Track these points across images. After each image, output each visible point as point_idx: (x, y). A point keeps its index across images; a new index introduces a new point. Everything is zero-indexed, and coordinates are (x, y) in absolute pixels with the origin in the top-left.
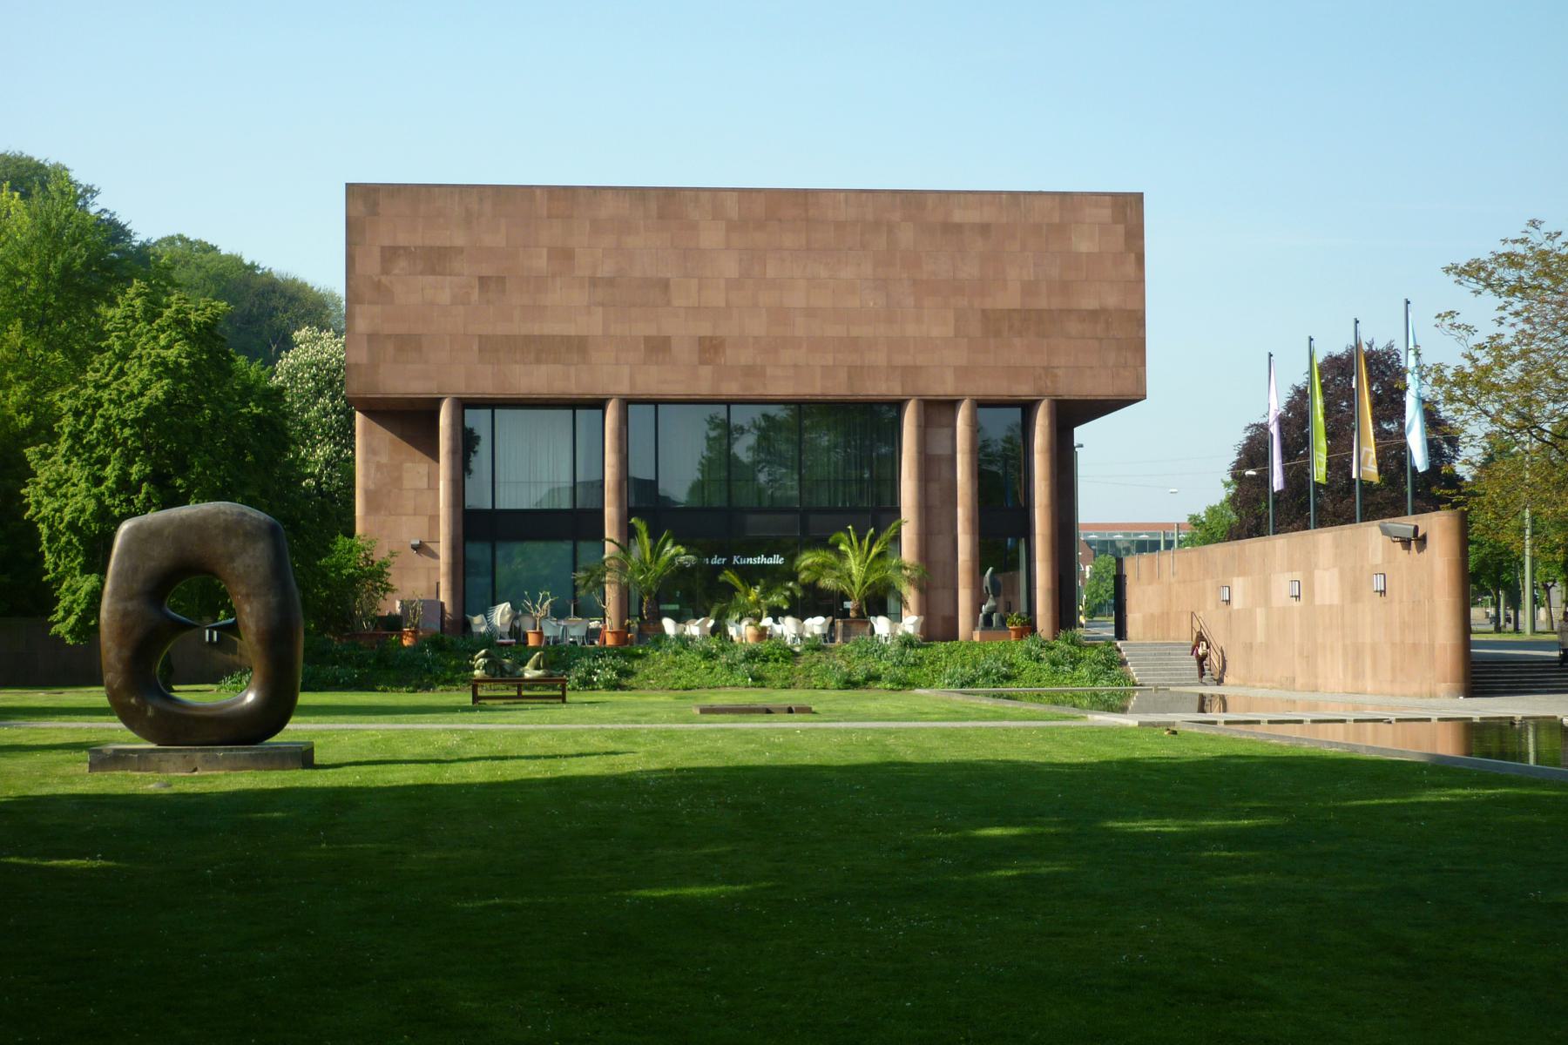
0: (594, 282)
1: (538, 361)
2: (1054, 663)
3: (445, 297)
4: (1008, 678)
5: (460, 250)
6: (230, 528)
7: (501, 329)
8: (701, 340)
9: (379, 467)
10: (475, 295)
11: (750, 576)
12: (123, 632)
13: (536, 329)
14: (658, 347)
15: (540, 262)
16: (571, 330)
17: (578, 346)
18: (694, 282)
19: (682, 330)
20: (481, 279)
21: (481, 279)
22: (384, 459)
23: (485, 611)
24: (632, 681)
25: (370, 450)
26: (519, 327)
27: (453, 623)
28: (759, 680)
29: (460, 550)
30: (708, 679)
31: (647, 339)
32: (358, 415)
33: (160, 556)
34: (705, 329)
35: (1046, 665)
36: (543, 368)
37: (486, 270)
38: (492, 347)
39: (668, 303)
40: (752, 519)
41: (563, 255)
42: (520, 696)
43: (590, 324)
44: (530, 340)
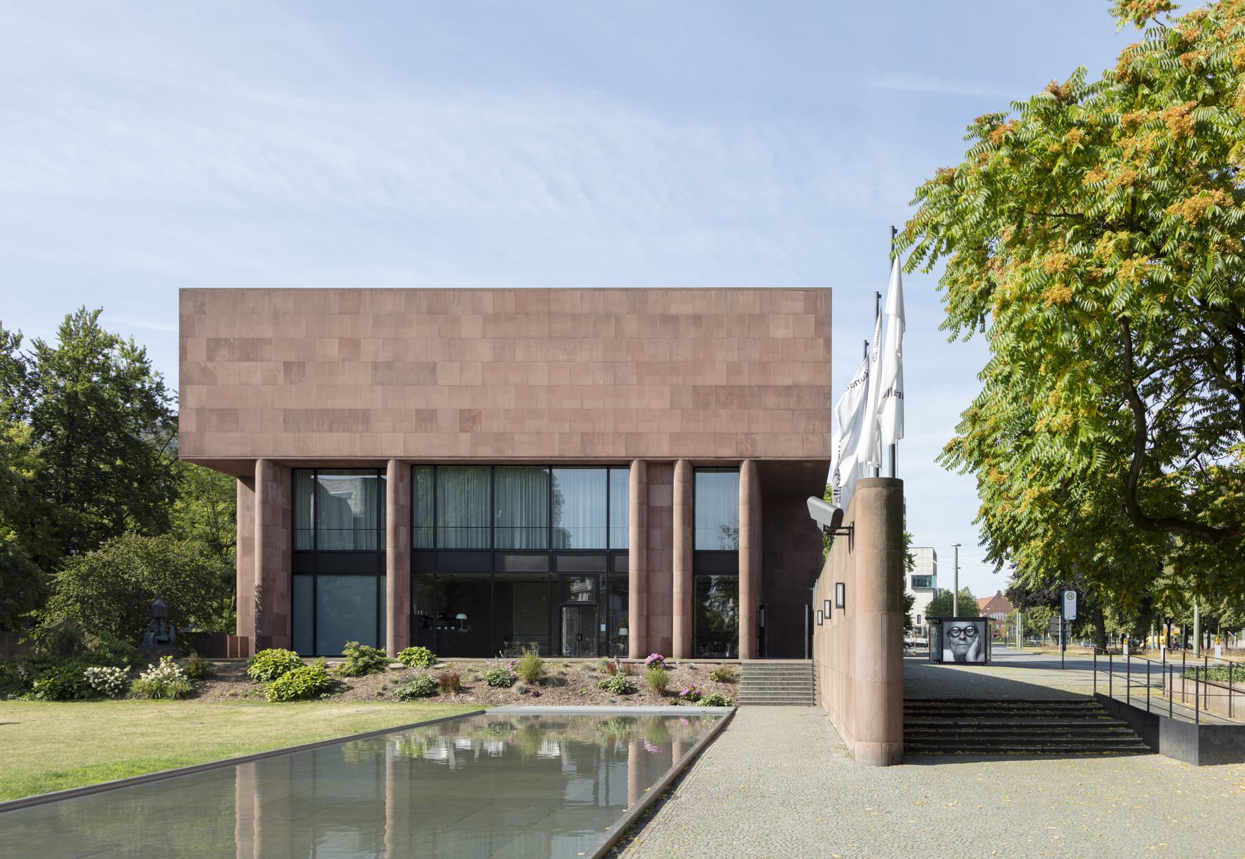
0: (376, 366)
5: (270, 341)
10: (281, 379)
13: (329, 405)
15: (332, 349)
16: (358, 405)
17: (362, 418)
19: (445, 403)
20: (287, 365)
21: (287, 365)
34: (465, 403)
38: (292, 419)
39: (435, 383)
41: (352, 344)
44: (323, 412)
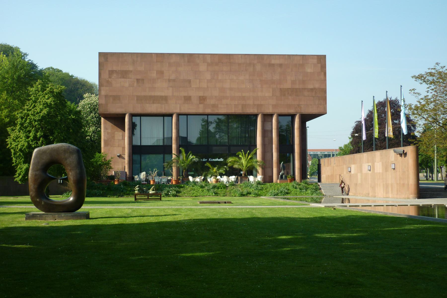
0: (169, 80)
1: (153, 103)
2: (300, 189)
3: (127, 85)
4: (287, 193)
5: (131, 71)
6: (66, 151)
7: (143, 94)
8: (200, 97)
9: (108, 133)
10: (135, 84)
11: (214, 164)
12: (35, 180)
13: (153, 94)
14: (188, 99)
15: (154, 75)
16: (163, 94)
17: (165, 99)
18: (198, 80)
19: (194, 94)
20: (137, 79)
21: (137, 79)
22: (109, 131)
23: (138, 174)
24: (180, 194)
25: (106, 128)
26: (148, 93)
27: (129, 178)
28: (216, 194)
29: (131, 157)
30: (202, 194)
31: (185, 97)
32: (102, 118)
33: (45, 159)
34: (201, 94)
35: (298, 190)
36: (155, 105)
37: (139, 77)
38: (140, 99)
39: (191, 86)
40: (215, 148)
41: (161, 73)
42: (148, 199)
43: (168, 93)
44: (151, 97)
